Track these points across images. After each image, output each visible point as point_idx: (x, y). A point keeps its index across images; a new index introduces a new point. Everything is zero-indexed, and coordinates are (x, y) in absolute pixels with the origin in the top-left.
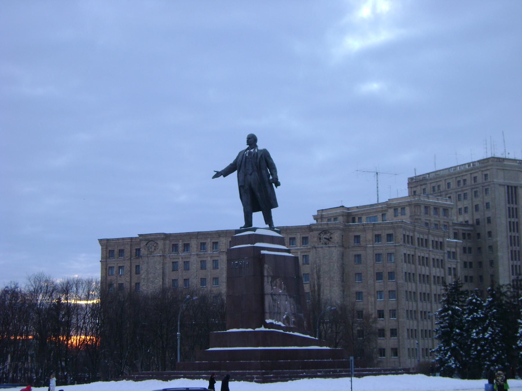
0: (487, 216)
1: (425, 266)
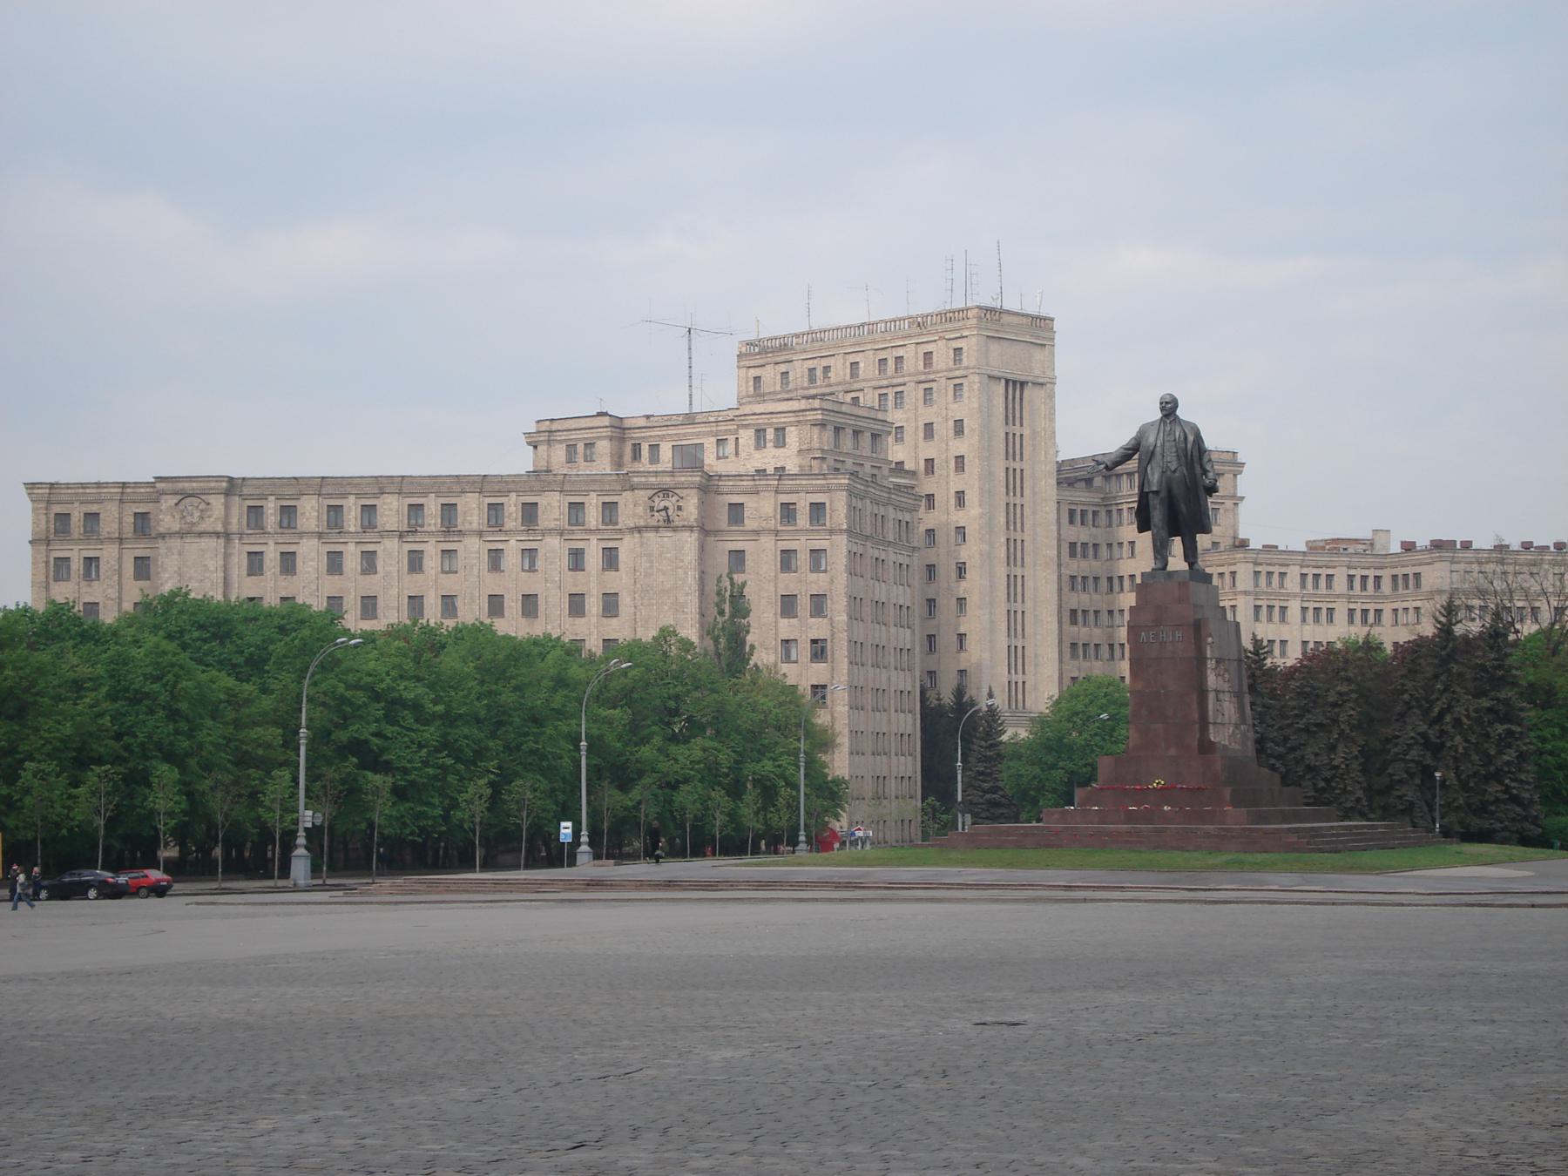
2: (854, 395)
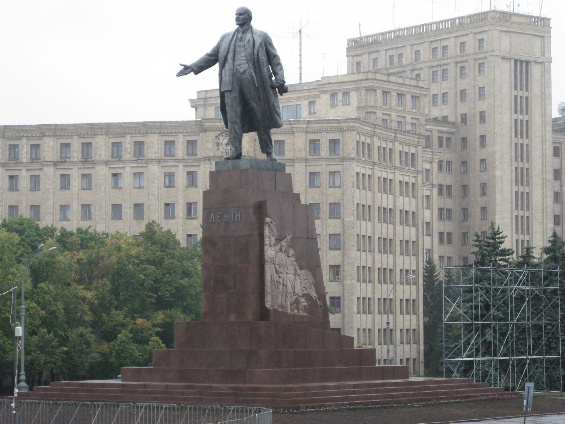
0: (479, 109)
1: (387, 194)
2: (417, 72)
